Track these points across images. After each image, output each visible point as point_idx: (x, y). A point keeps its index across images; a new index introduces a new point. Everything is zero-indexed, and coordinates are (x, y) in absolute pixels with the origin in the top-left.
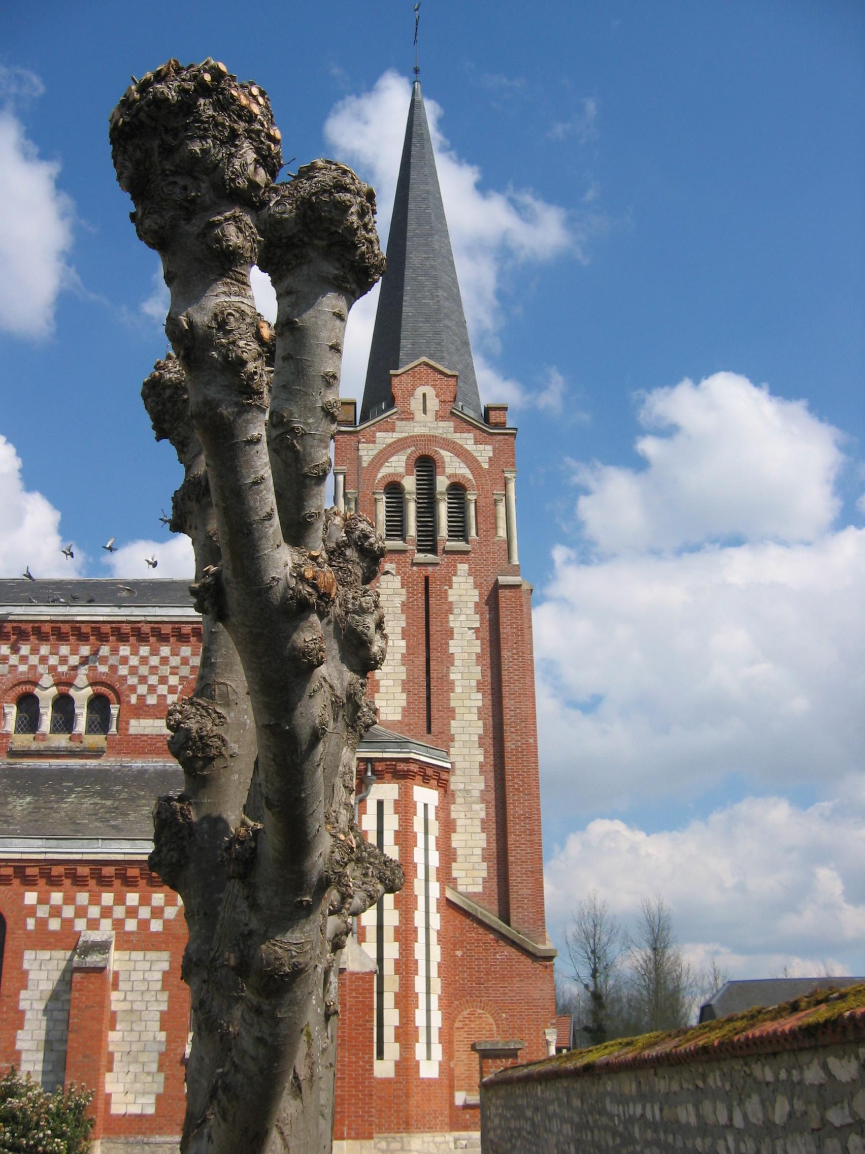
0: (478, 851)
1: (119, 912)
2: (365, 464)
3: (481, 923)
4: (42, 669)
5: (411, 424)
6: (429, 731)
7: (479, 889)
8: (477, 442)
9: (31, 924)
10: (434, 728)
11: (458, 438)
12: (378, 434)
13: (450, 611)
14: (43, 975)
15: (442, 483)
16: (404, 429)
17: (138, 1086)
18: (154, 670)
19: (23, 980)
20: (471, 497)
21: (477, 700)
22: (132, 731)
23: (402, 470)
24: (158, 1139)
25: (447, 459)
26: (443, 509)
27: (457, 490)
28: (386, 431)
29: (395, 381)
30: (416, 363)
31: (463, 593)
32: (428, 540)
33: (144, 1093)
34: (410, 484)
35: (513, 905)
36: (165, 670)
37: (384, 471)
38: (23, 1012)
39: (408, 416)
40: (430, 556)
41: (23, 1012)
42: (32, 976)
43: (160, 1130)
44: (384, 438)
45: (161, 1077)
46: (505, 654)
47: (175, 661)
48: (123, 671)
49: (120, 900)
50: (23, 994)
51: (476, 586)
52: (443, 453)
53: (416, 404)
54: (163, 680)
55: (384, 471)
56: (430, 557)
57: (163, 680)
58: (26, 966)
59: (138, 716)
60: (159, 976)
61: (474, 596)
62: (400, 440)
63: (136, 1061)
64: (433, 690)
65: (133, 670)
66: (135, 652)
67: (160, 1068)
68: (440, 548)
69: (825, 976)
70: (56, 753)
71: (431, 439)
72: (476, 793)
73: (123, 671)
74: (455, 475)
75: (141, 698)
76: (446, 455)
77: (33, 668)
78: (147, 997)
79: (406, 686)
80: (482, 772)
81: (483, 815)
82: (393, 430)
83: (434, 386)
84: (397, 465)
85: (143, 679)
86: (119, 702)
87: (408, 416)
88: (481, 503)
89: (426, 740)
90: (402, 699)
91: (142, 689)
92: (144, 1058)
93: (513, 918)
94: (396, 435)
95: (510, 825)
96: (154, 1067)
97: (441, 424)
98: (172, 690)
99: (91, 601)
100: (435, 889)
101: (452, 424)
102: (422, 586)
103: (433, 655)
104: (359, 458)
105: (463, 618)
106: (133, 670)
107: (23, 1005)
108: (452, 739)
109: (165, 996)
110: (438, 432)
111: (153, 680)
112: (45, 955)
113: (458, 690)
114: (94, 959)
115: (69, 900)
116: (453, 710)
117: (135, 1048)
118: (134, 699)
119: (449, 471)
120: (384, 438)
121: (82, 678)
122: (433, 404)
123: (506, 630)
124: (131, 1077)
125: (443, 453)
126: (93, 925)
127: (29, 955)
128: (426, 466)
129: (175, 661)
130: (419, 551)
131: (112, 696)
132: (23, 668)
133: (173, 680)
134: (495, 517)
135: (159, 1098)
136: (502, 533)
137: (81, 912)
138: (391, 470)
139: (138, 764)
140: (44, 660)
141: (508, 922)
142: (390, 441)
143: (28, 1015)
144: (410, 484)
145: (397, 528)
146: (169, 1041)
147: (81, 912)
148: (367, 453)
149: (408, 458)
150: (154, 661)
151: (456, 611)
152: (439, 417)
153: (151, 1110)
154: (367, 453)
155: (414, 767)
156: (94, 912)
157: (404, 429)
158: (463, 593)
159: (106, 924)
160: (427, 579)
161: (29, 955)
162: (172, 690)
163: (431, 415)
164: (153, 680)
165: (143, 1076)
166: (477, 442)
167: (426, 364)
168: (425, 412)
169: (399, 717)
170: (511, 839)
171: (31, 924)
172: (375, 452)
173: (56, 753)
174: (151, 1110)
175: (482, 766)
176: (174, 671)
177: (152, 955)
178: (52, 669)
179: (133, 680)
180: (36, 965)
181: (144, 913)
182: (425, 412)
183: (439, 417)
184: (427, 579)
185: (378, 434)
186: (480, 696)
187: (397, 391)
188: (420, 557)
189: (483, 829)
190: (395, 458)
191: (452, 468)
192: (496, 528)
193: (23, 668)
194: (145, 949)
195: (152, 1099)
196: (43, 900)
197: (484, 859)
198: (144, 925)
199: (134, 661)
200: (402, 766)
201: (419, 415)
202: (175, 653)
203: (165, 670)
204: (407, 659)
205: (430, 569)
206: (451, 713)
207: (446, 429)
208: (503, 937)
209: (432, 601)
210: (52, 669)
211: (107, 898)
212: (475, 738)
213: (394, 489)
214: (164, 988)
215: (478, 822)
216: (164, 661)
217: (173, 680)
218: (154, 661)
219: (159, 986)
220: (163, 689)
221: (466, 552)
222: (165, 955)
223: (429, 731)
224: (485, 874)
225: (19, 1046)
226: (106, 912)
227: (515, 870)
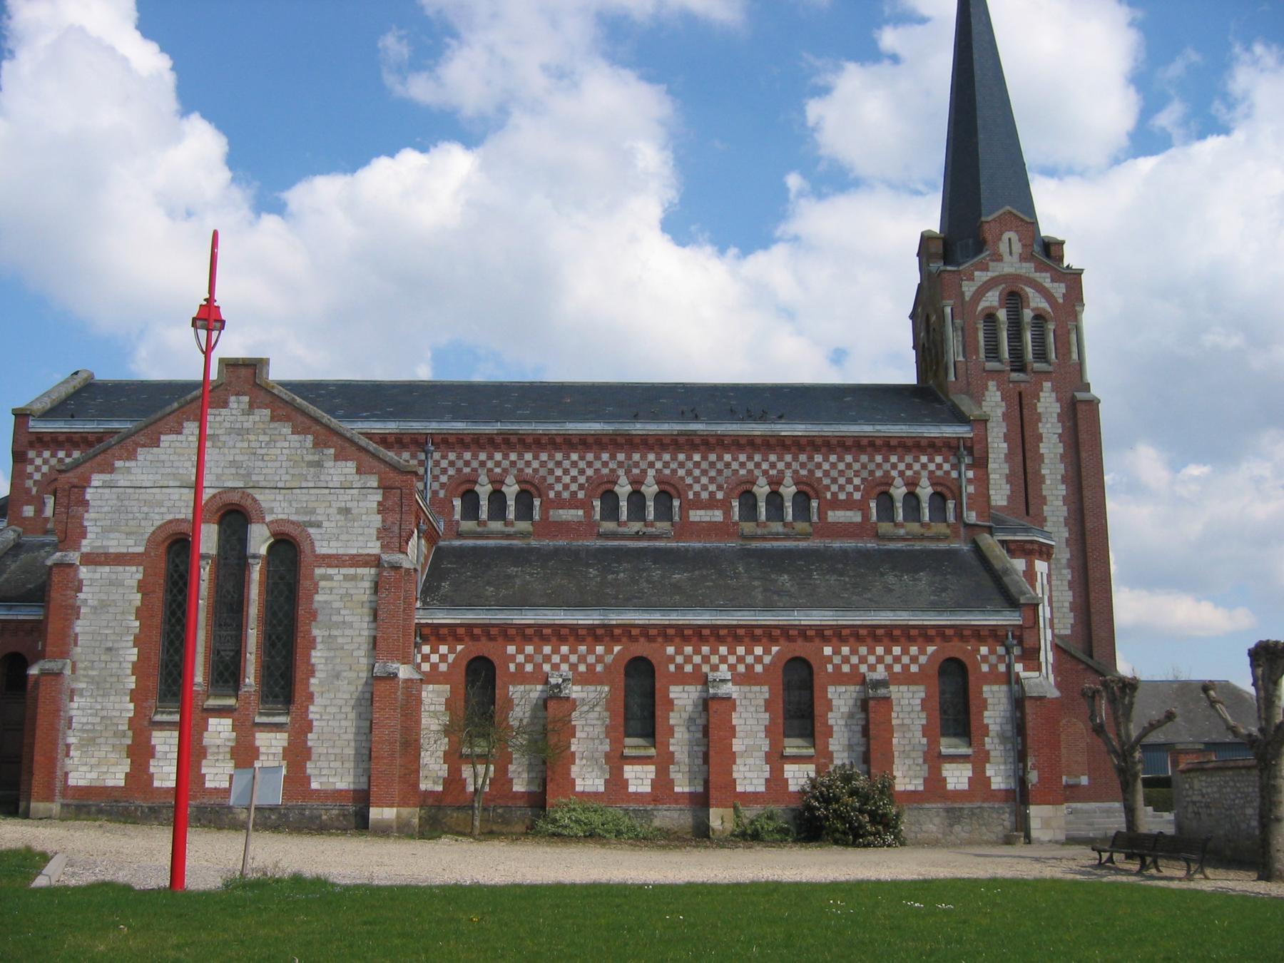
0: (1067, 605)
1: (889, 659)
2: (967, 299)
3: (1073, 657)
4: (757, 472)
5: (1000, 264)
6: (1028, 513)
7: (1068, 632)
8: (1053, 281)
9: (830, 668)
10: (1031, 512)
11: (1048, 284)
12: (976, 273)
13: (1039, 420)
14: (842, 702)
15: (1028, 315)
16: (996, 270)
17: (911, 773)
18: (841, 473)
19: (829, 707)
20: (1051, 326)
21: (1062, 490)
22: (830, 520)
23: (996, 304)
24: (927, 806)
25: (1031, 295)
26: (1028, 336)
27: (1040, 318)
28: (982, 270)
29: (986, 227)
30: (1001, 211)
31: (1048, 404)
32: (1019, 364)
33: (916, 777)
34: (1002, 315)
35: (1095, 644)
36: (850, 473)
37: (982, 305)
38: (831, 727)
39: (998, 258)
40: (1021, 375)
41: (831, 727)
42: (834, 702)
43: (928, 800)
44: (981, 277)
45: (926, 767)
46: (1083, 455)
47: (857, 466)
48: (819, 474)
49: (888, 651)
50: (830, 715)
51: (1058, 400)
52: (1028, 290)
53: (1003, 247)
54: (849, 481)
55: (982, 305)
56: (1021, 376)
57: (849, 481)
58: (830, 696)
59: (834, 509)
60: (919, 701)
61: (1056, 408)
62: (993, 279)
63: (908, 757)
64: (1030, 482)
65: (826, 473)
66: (826, 459)
67: (925, 761)
68: (1029, 368)
69: (1130, 676)
70: (776, 537)
71: (1017, 278)
72: (1064, 561)
73: (819, 474)
74: (1037, 309)
75: (834, 494)
76: (1029, 290)
77: (750, 472)
78: (913, 715)
79: (1009, 478)
80: (1068, 545)
81: (1069, 577)
82: (987, 270)
83: (1017, 232)
84: (992, 299)
85: (834, 481)
86: (818, 497)
87: (998, 258)
88: (1058, 333)
89: (1026, 522)
90: (1006, 489)
91: (834, 488)
92: (913, 755)
93: (1095, 654)
94: (990, 274)
95: (1091, 585)
96: (921, 761)
97: (1024, 265)
98: (857, 488)
99: (780, 417)
100: (1049, 632)
101: (1048, 275)
102: (1017, 399)
103: (1028, 455)
104: (963, 294)
105: (1049, 425)
106: (826, 473)
107: (831, 722)
108: (1045, 520)
109: (923, 715)
110: (1023, 272)
111: (842, 481)
112: (843, 689)
113: (1048, 482)
114: (882, 692)
115: (854, 652)
116: (1045, 498)
117: (907, 748)
118: (829, 496)
119: (1033, 305)
120: (981, 277)
121: (788, 480)
122: (1017, 248)
123: (1083, 436)
124: (906, 767)
125: (1028, 290)
126: (872, 668)
127: (831, 689)
128: (1014, 299)
129: (857, 466)
130: (1012, 370)
131: (812, 493)
132: (743, 472)
133: (857, 481)
134: (1069, 343)
135: (925, 780)
136: (1075, 356)
137: (863, 660)
138: (987, 304)
139: (837, 544)
140: (758, 465)
141: (1091, 656)
142: (985, 279)
143: (835, 729)
144: (1002, 315)
145: (993, 352)
146: (929, 744)
147: (863, 660)
148: (969, 289)
149: (1044, 309)
150: (841, 466)
151: (1044, 420)
152: (1023, 258)
153: (921, 788)
154: (969, 289)
155: (1036, 547)
156: (872, 659)
157: (996, 270)
158: (1048, 404)
159: (880, 668)
160: (1020, 394)
161: (831, 689)
162: (857, 488)
163: (1016, 258)
164: (842, 481)
165: (914, 767)
166: (1053, 281)
167: (1010, 212)
168: (1011, 253)
169: (1005, 503)
170: (1092, 595)
171: (830, 668)
172: (974, 289)
173: (776, 537)
174: (921, 788)
175: (1067, 540)
176: (857, 474)
177: (912, 688)
178: (765, 473)
179: (826, 481)
180: (836, 696)
181: (906, 660)
182: (1011, 253)
183: (1023, 258)
184: (1020, 394)
185: (976, 273)
186: (1064, 487)
187: (989, 237)
188: (1014, 376)
189: (1070, 588)
190: (990, 294)
191: (1037, 301)
192: (1069, 352)
193: (743, 472)
194: (908, 684)
195: (921, 781)
196: (836, 652)
197: (1071, 610)
198: (906, 668)
199: (826, 466)
200: (1028, 546)
201: (1006, 257)
202: (856, 460)
203: (850, 473)
204: (1009, 457)
205: (1022, 385)
206: (1043, 500)
207: (1027, 269)
208: (1089, 667)
209: (1025, 411)
210: (765, 473)
211: (880, 650)
212: (1062, 519)
213: (990, 317)
214: (923, 710)
215: (1066, 583)
216: (849, 466)
217: (857, 481)
218: (841, 466)
219: (919, 708)
220: (850, 488)
221: (1049, 372)
222: (922, 688)
223: (1028, 513)
224: (1072, 621)
225: (831, 748)
226: (880, 660)
227: (1095, 618)
